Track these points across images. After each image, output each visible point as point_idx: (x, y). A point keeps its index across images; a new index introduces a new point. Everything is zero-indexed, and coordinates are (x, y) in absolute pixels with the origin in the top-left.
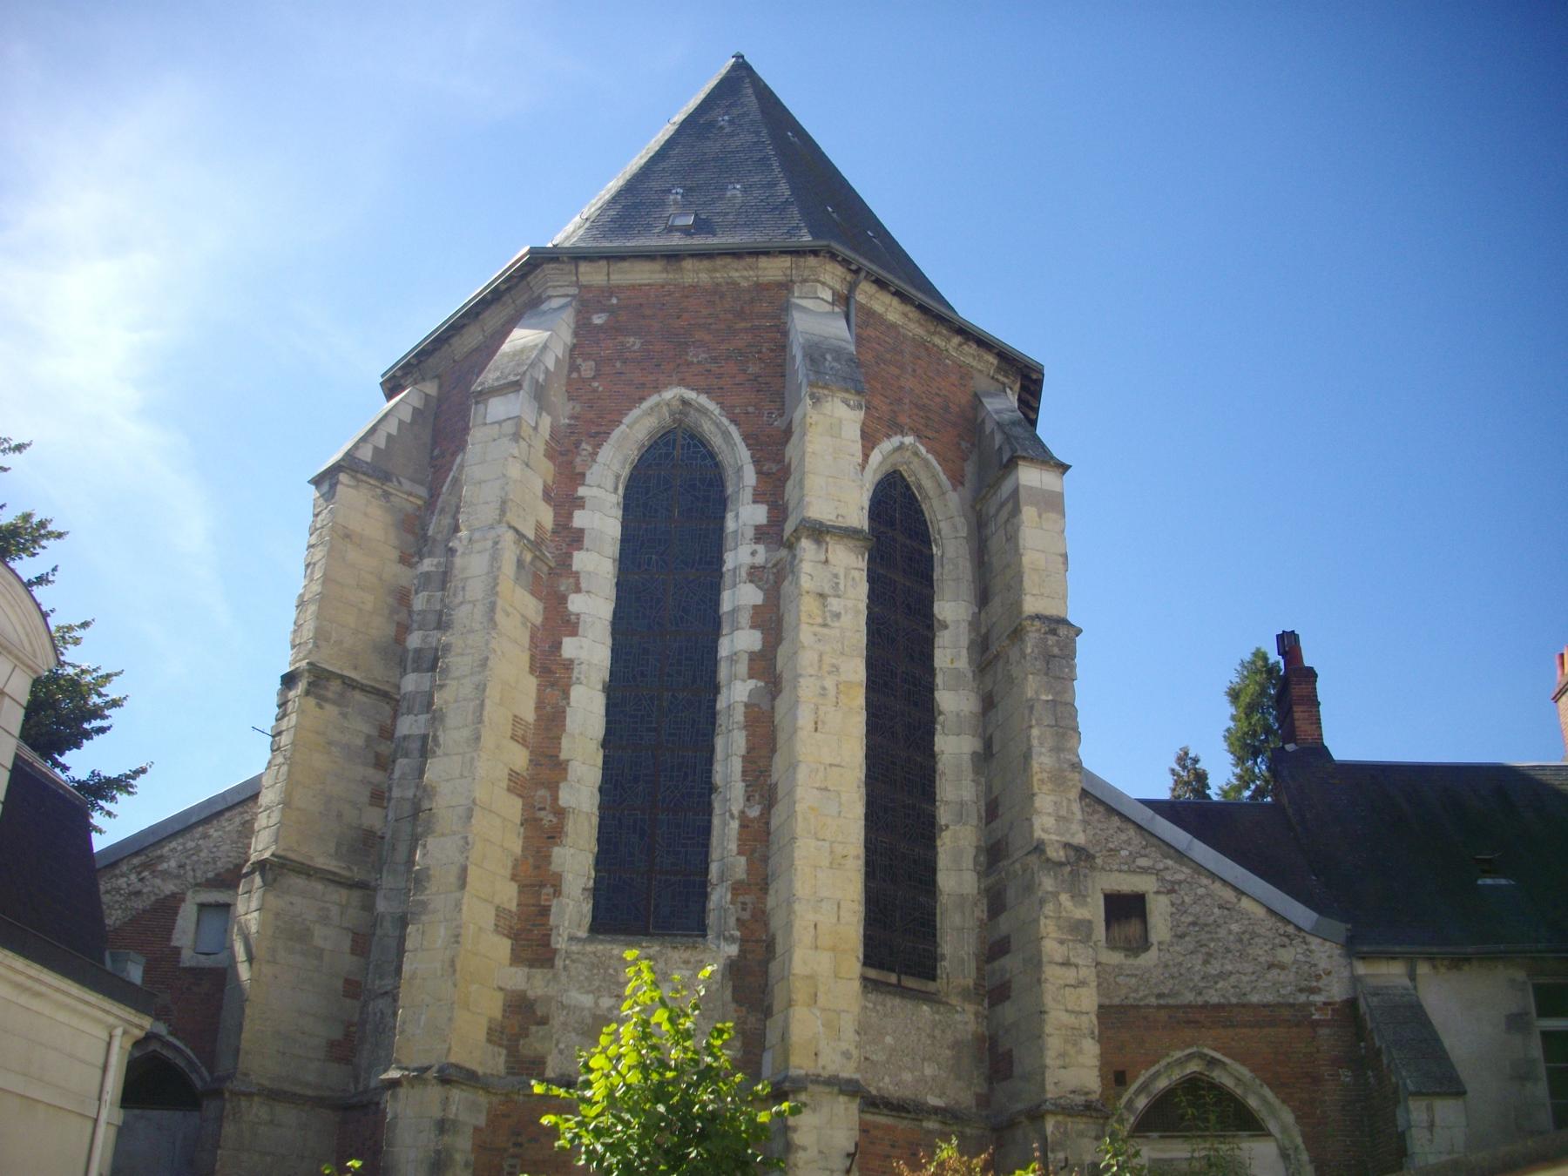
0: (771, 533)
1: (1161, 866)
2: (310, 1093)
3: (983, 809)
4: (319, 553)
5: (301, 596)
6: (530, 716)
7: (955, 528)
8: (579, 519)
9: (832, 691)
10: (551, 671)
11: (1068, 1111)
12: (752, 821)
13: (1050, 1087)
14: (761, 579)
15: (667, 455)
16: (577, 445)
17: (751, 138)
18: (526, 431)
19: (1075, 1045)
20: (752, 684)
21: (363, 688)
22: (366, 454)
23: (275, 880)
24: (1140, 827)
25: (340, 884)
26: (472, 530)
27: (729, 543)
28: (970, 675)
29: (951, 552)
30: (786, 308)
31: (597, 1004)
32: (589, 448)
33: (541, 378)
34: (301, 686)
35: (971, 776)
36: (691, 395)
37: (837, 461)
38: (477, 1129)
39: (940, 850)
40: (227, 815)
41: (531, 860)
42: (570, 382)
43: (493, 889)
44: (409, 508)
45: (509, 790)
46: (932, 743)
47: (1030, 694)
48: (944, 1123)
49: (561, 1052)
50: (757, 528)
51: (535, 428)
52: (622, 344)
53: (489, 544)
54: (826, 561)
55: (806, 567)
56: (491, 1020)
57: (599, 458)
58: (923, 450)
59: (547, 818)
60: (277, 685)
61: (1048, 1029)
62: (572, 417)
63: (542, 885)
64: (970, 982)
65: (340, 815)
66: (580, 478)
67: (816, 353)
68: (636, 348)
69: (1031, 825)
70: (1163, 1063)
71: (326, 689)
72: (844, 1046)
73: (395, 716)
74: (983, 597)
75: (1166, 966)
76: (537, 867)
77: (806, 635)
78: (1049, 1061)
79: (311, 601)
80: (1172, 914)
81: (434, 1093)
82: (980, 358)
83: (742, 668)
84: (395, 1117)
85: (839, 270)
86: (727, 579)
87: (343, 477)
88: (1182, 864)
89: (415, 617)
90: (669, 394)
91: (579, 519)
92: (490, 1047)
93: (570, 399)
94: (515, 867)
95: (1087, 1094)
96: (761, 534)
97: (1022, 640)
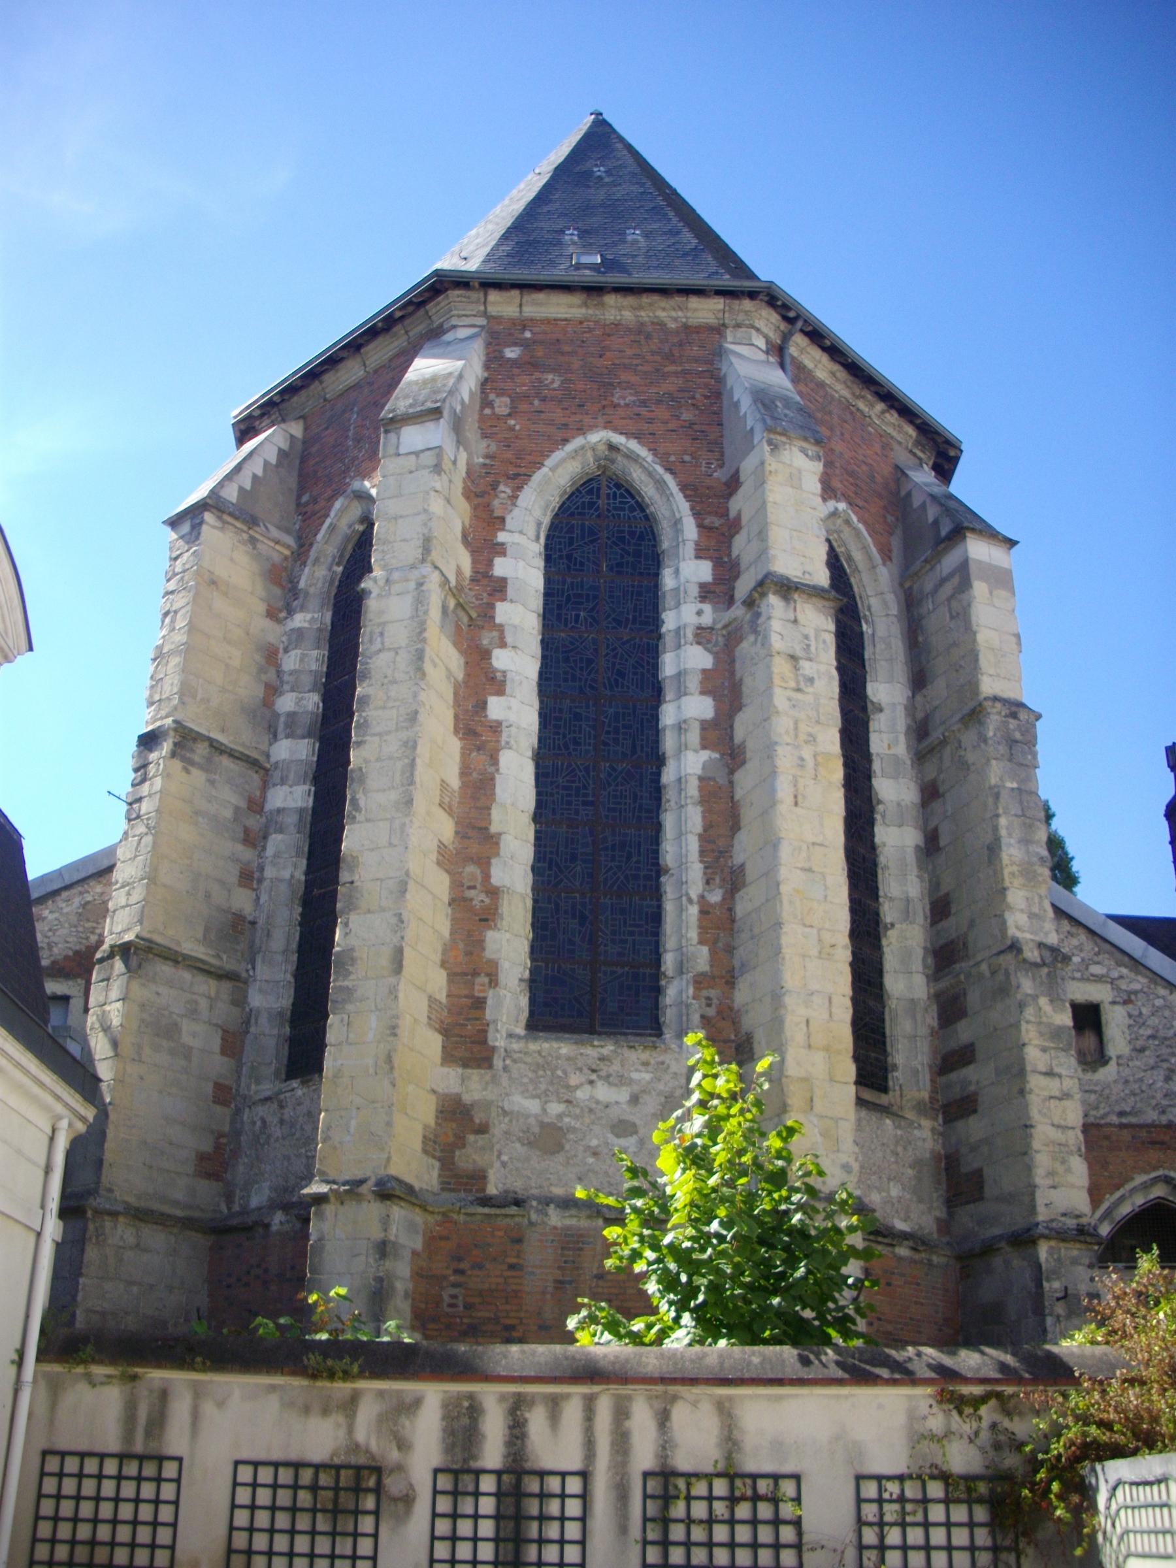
0: (719, 591)
1: (1115, 974)
2: (179, 1213)
3: (928, 907)
4: (180, 601)
5: (159, 648)
6: (455, 782)
7: (885, 604)
8: (501, 567)
9: (810, 763)
10: (477, 733)
11: (1061, 1235)
12: (711, 905)
13: (1041, 1209)
14: (709, 641)
15: (592, 504)
16: (494, 486)
17: (636, 189)
18: (447, 465)
19: (1063, 1162)
20: (705, 755)
21: (232, 754)
22: (231, 494)
23: (140, 966)
24: (1091, 932)
25: (208, 973)
26: (390, 570)
27: (669, 601)
28: (909, 762)
29: (881, 631)
30: (719, 353)
31: (544, 1110)
32: (508, 491)
33: (459, 408)
34: (166, 747)
35: (915, 872)
36: (619, 439)
37: (794, 511)
38: (415, 1253)
39: (886, 950)
40: (65, 894)
41: (461, 946)
42: (482, 419)
43: (426, 980)
44: (276, 558)
45: (439, 863)
46: (872, 835)
47: (993, 780)
48: (914, 1249)
49: (504, 1164)
50: (702, 586)
51: (454, 463)
52: (540, 381)
53: (412, 585)
54: (795, 621)
55: (776, 625)
56: (426, 1127)
57: (519, 502)
58: (855, 519)
59: (478, 898)
60: (132, 745)
61: (1036, 1144)
62: (487, 456)
63: (475, 974)
64: (925, 1095)
65: (208, 896)
66: (499, 522)
67: (764, 399)
68: (556, 385)
69: (1004, 923)
70: (1128, 1186)
71: (192, 751)
72: (844, 1158)
73: (265, 786)
74: (919, 680)
75: (1127, 1082)
76: (469, 954)
77: (780, 698)
78: (1038, 1180)
79: (171, 653)
80: (1130, 1026)
81: (372, 1210)
82: (900, 429)
83: (694, 736)
84: (321, 1239)
85: (774, 317)
86: (669, 640)
87: (208, 517)
88: (1138, 973)
89: (286, 678)
90: (597, 437)
91: (501, 567)
92: (425, 1158)
93: (485, 436)
94: (444, 952)
95: (1078, 1216)
96: (706, 593)
97: (981, 723)
